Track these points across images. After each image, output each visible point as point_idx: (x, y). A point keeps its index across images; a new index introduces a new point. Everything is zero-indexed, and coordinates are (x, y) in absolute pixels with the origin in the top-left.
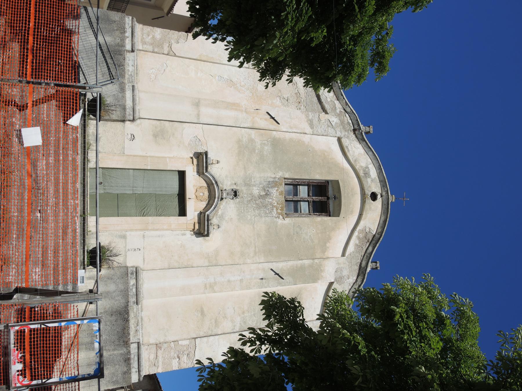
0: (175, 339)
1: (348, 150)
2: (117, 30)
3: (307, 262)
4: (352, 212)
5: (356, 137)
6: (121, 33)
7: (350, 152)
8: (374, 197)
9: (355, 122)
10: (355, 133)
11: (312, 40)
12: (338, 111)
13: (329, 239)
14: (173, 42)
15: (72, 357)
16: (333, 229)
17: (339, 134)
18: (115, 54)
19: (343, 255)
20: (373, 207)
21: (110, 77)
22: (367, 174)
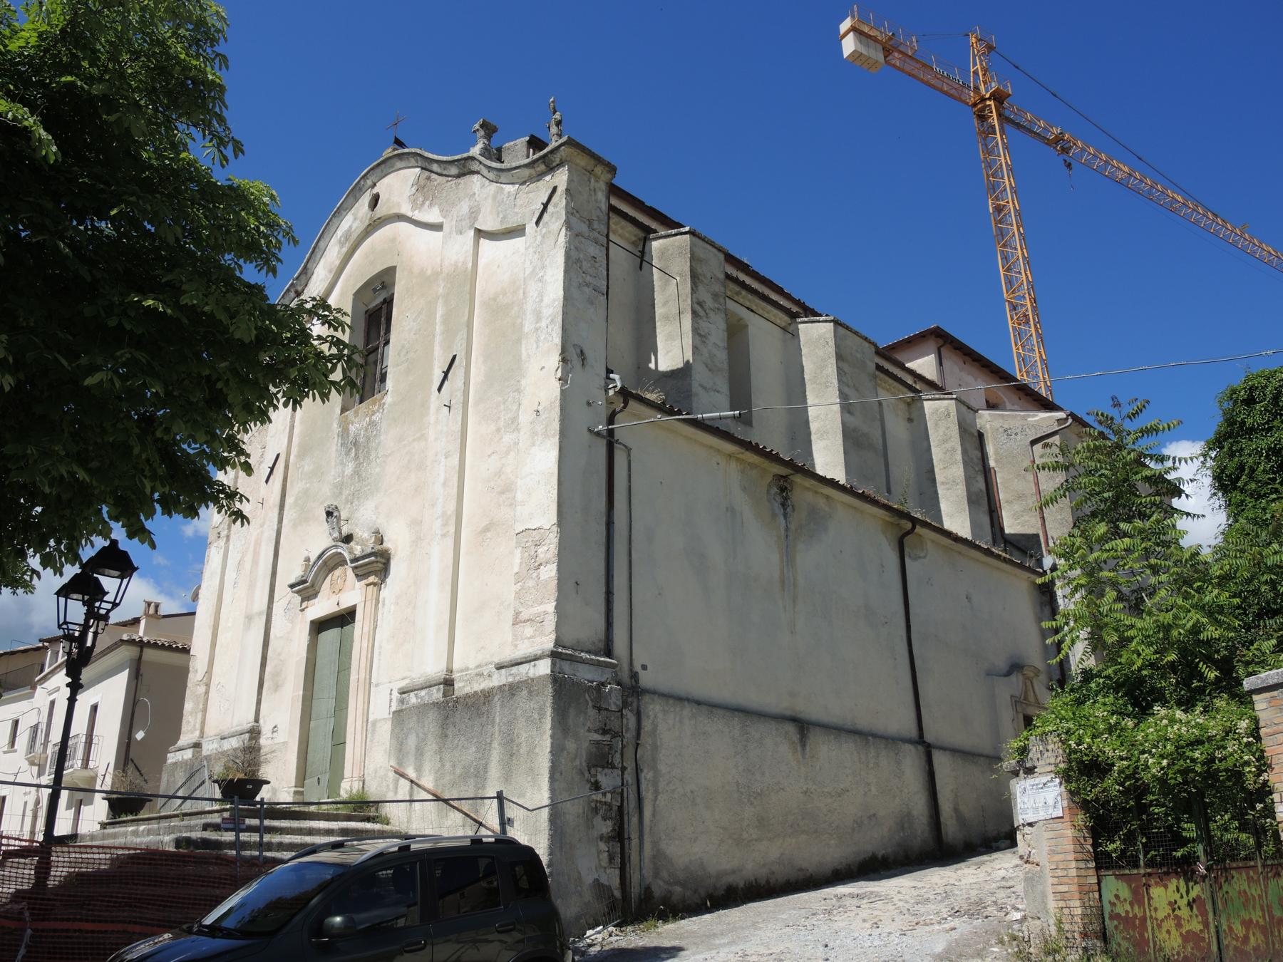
19: (437, 227)
22: (347, 236)
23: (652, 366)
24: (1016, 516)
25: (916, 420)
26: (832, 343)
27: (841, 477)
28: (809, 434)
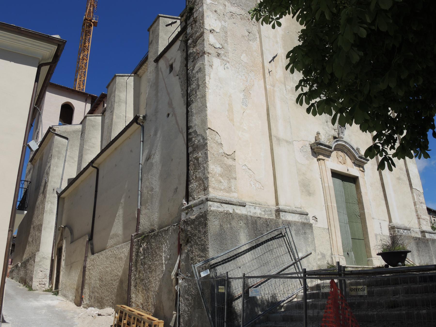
0: (413, 204)
2: (230, 224)
6: (233, 218)
14: (221, 151)
15: (282, 251)
18: (257, 229)
21: (280, 237)
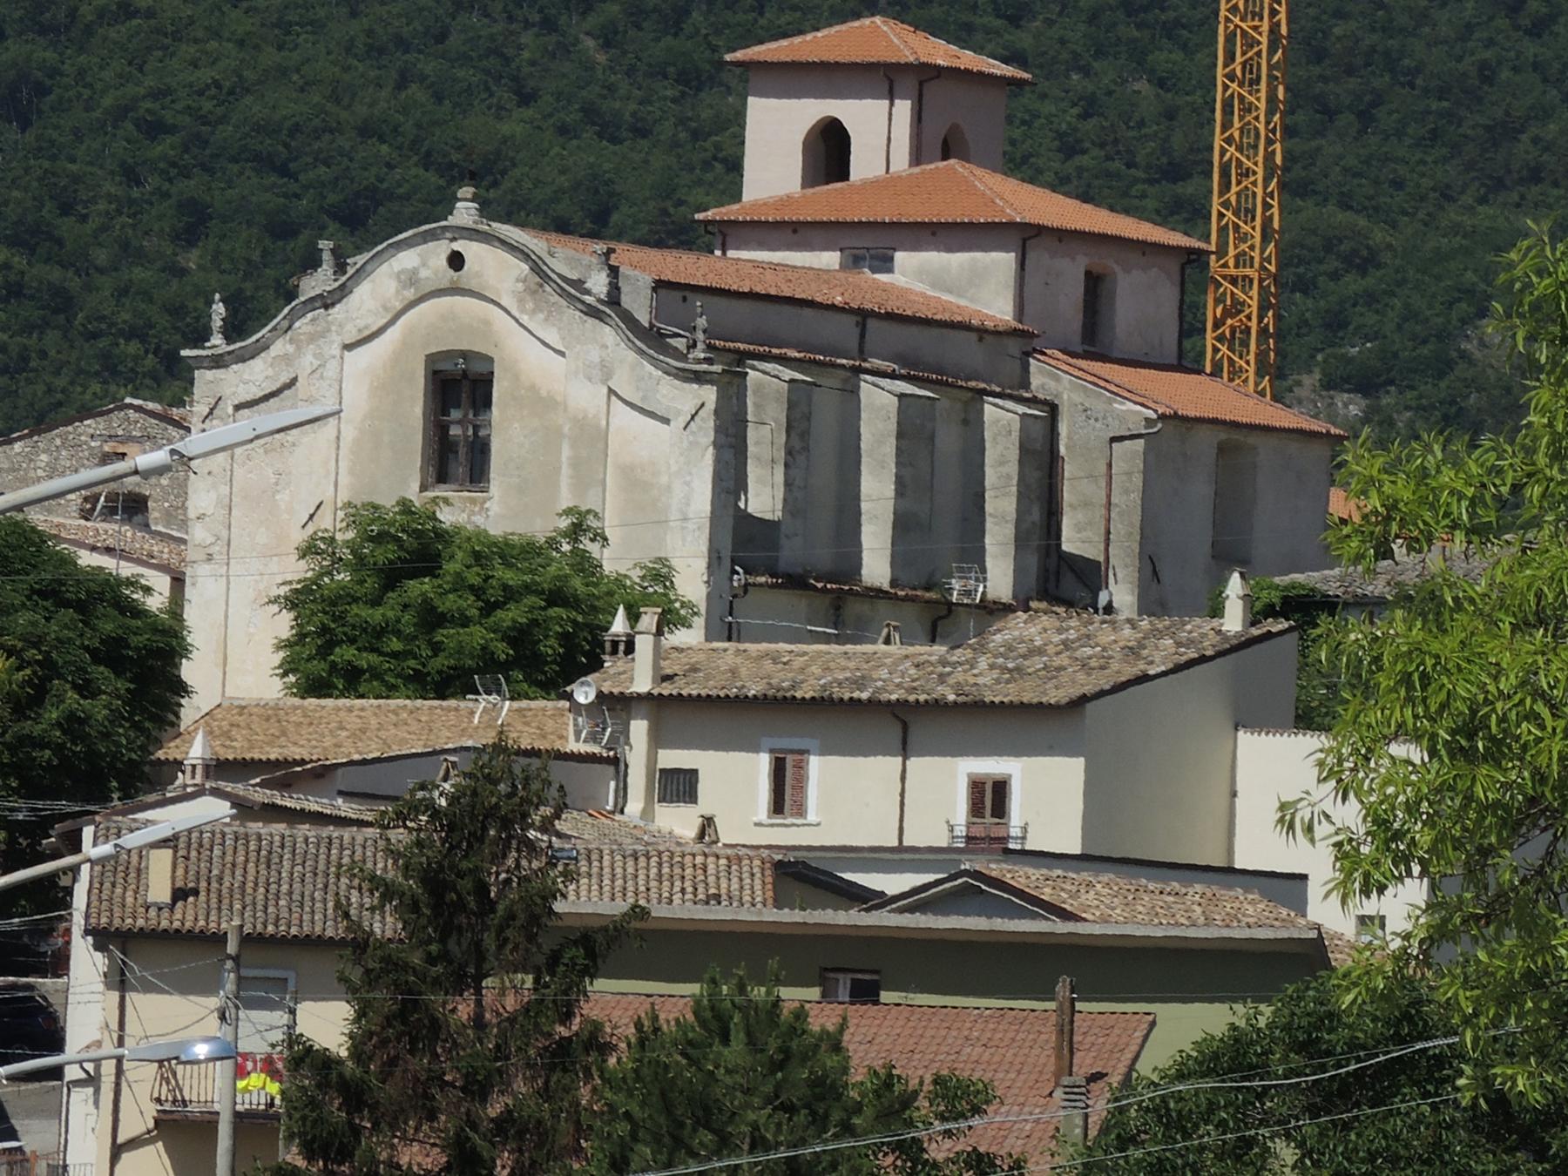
1: (366, 327)
3: (566, 452)
4: (487, 323)
5: (339, 301)
7: (370, 321)
8: (456, 261)
9: (309, 307)
10: (333, 305)
11: (128, 690)
12: (290, 349)
13: (533, 388)
16: (516, 377)
17: (336, 351)
19: (562, 354)
20: (476, 268)
22: (411, 278)
23: (742, 505)
24: (1079, 528)
25: (972, 424)
26: (894, 420)
27: (644, 318)
28: (859, 514)
